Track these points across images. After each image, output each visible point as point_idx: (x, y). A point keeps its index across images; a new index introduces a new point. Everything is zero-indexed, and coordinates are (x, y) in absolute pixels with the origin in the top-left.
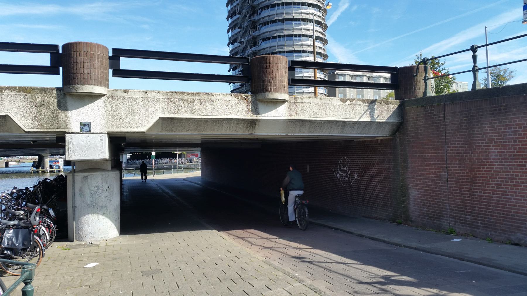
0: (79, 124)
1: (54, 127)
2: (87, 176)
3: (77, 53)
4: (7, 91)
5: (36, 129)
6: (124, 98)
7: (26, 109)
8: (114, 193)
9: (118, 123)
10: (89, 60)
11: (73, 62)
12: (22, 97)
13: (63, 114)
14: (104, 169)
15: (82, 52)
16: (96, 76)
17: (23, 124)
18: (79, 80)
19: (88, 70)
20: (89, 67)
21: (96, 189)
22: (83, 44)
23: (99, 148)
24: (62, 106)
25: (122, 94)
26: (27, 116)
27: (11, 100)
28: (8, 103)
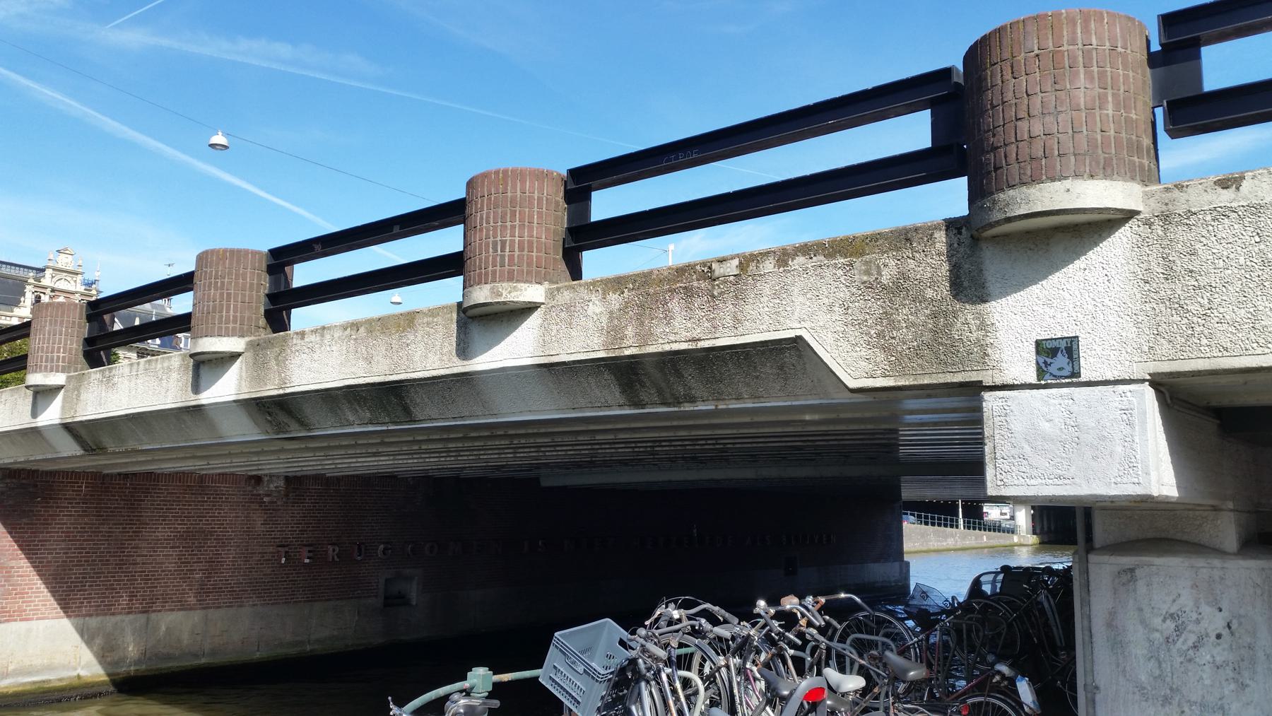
0: (1032, 348)
1: (942, 367)
2: (1132, 570)
3: (1004, 68)
4: (801, 259)
5: (881, 379)
6: (1221, 213)
7: (850, 311)
8: (1261, 654)
9: (1198, 329)
10: (1050, 81)
11: (992, 104)
12: (840, 272)
13: (970, 317)
14: (1207, 547)
15: (1021, 57)
16: (1082, 140)
17: (841, 363)
18: (1015, 168)
19: (1048, 119)
20: (1052, 110)
21: (1170, 625)
22: (1021, 26)
23: (1119, 449)
24: (966, 284)
25: (1207, 197)
26: (853, 333)
27: (810, 285)
28: (801, 299)
